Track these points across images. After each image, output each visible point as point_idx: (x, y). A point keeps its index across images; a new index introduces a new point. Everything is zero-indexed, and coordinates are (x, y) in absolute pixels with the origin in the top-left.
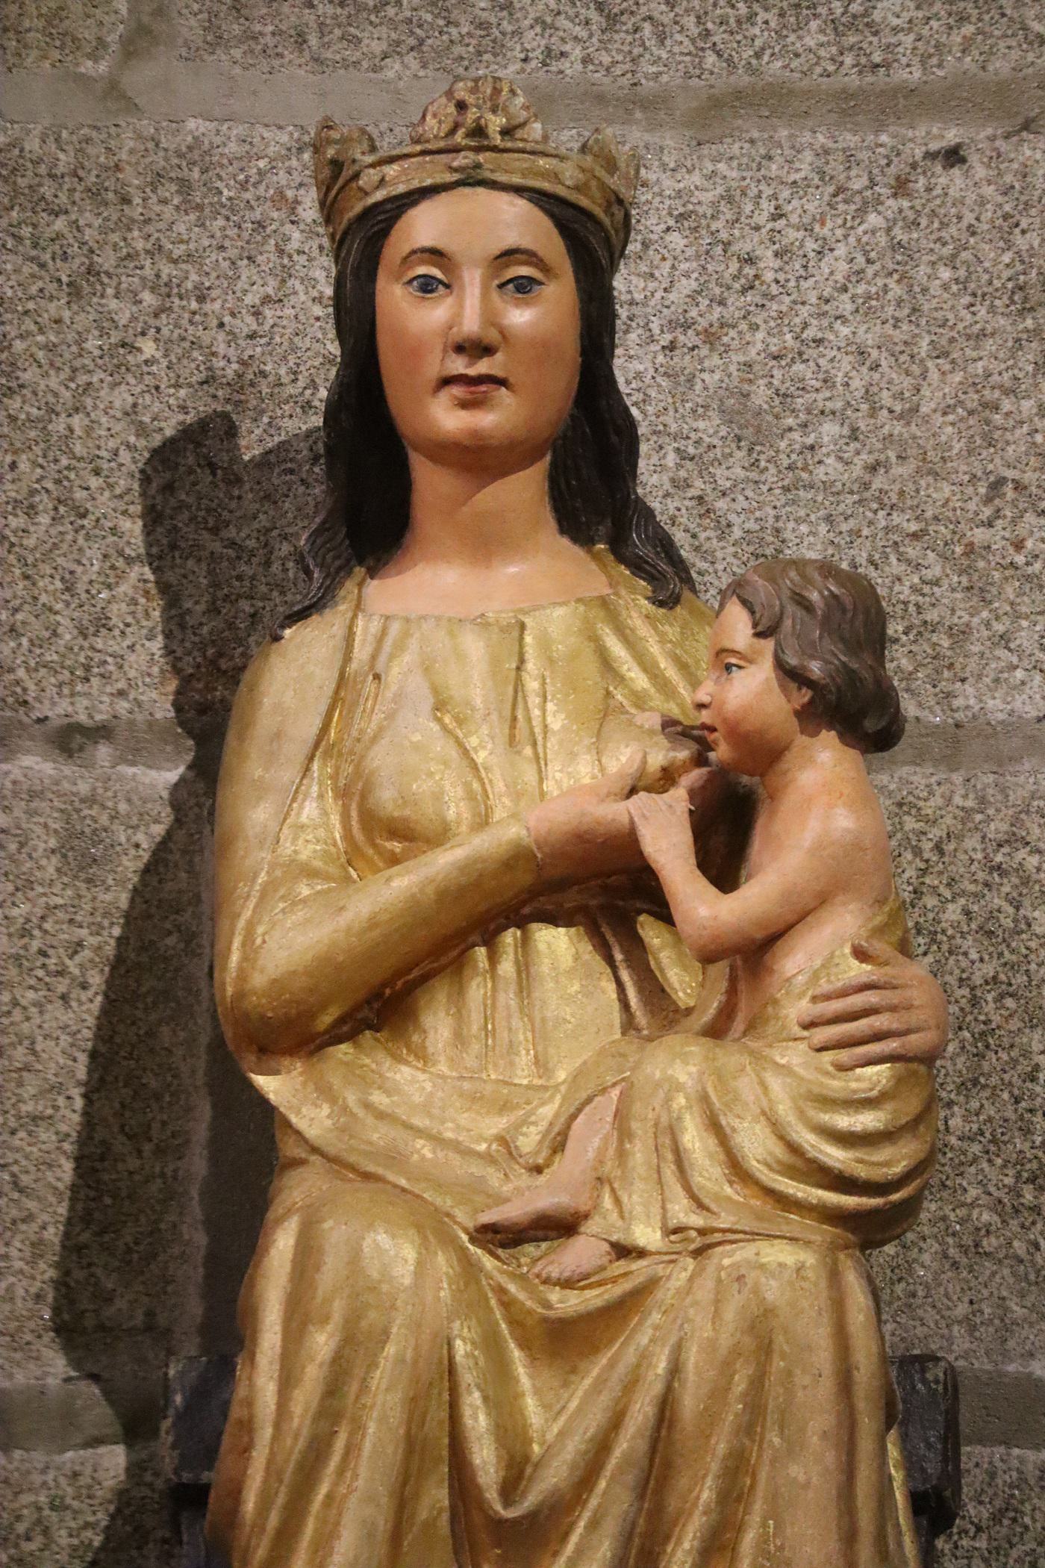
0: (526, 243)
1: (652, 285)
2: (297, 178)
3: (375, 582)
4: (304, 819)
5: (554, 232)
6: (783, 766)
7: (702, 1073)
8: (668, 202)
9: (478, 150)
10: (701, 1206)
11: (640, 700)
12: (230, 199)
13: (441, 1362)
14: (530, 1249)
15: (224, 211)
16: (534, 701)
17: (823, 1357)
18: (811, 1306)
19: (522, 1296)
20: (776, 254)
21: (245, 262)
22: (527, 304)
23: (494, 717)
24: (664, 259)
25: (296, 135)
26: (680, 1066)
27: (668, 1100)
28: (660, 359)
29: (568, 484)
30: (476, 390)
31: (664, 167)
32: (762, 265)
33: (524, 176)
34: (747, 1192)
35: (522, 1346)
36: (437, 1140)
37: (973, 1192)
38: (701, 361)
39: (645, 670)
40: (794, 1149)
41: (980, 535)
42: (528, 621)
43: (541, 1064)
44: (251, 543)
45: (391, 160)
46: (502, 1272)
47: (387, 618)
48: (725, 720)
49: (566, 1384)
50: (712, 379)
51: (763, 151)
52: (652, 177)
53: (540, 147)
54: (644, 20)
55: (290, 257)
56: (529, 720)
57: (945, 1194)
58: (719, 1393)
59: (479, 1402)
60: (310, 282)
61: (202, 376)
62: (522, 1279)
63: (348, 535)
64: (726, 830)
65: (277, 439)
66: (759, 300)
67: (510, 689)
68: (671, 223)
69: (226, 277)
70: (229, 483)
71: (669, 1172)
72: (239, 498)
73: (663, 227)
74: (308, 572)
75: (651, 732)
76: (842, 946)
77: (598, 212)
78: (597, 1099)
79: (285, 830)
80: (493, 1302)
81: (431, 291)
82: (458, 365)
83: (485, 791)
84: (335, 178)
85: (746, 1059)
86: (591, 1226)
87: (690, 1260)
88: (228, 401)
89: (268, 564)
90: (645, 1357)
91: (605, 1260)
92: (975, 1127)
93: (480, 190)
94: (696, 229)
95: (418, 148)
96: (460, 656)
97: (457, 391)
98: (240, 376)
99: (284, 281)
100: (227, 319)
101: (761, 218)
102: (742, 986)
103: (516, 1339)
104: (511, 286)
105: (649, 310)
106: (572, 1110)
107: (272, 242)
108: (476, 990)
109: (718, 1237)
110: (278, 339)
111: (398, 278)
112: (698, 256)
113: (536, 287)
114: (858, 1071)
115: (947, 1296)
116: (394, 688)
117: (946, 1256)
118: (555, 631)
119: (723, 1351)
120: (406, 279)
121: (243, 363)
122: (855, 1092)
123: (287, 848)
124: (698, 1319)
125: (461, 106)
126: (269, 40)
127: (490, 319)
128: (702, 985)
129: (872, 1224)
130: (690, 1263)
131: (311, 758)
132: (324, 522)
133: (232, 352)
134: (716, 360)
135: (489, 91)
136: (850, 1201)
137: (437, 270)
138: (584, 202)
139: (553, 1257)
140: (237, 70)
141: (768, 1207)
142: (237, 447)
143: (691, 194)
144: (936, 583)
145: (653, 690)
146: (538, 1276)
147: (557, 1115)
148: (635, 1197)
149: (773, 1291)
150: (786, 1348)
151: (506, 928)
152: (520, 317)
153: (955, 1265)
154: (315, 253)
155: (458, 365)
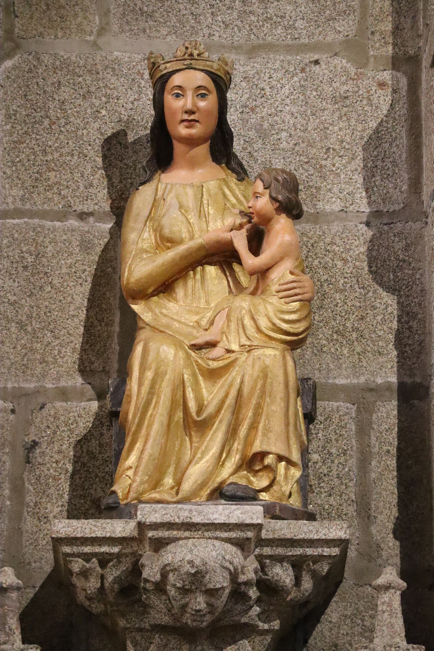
0: (203, 84)
1: (237, 96)
4: (144, 237)
5: (211, 82)
9: (191, 60)
11: (233, 206)
14: (204, 350)
16: (206, 206)
17: (281, 379)
19: (202, 363)
22: (204, 100)
23: (195, 210)
26: (244, 303)
27: (241, 312)
28: (239, 115)
30: (191, 123)
36: (180, 322)
37: (321, 336)
38: (250, 116)
39: (235, 198)
40: (274, 324)
41: (323, 163)
42: (204, 185)
43: (207, 302)
44: (131, 164)
49: (213, 386)
52: (237, 67)
56: (204, 211)
57: (313, 336)
58: (253, 388)
64: (255, 246)
68: (242, 79)
71: (241, 331)
74: (146, 172)
75: (236, 214)
77: (223, 76)
79: (140, 240)
80: (194, 364)
82: (186, 117)
84: (153, 67)
85: (261, 301)
86: (220, 345)
89: (135, 170)
90: (234, 379)
91: (224, 354)
93: (192, 70)
95: (175, 59)
96: (186, 194)
97: (185, 123)
99: (140, 95)
100: (125, 105)
101: (266, 78)
102: (260, 281)
103: (200, 374)
108: (190, 283)
109: (254, 347)
112: (249, 88)
119: (255, 377)
121: (129, 116)
123: (140, 245)
125: (187, 48)
127: (194, 104)
128: (250, 281)
130: (246, 354)
131: (146, 221)
133: (126, 114)
136: (289, 338)
138: (219, 74)
140: (128, 39)
141: (267, 340)
142: (127, 139)
144: (312, 175)
147: (211, 315)
149: (268, 362)
152: (202, 104)
153: (316, 355)
154: (148, 87)
155: (186, 117)
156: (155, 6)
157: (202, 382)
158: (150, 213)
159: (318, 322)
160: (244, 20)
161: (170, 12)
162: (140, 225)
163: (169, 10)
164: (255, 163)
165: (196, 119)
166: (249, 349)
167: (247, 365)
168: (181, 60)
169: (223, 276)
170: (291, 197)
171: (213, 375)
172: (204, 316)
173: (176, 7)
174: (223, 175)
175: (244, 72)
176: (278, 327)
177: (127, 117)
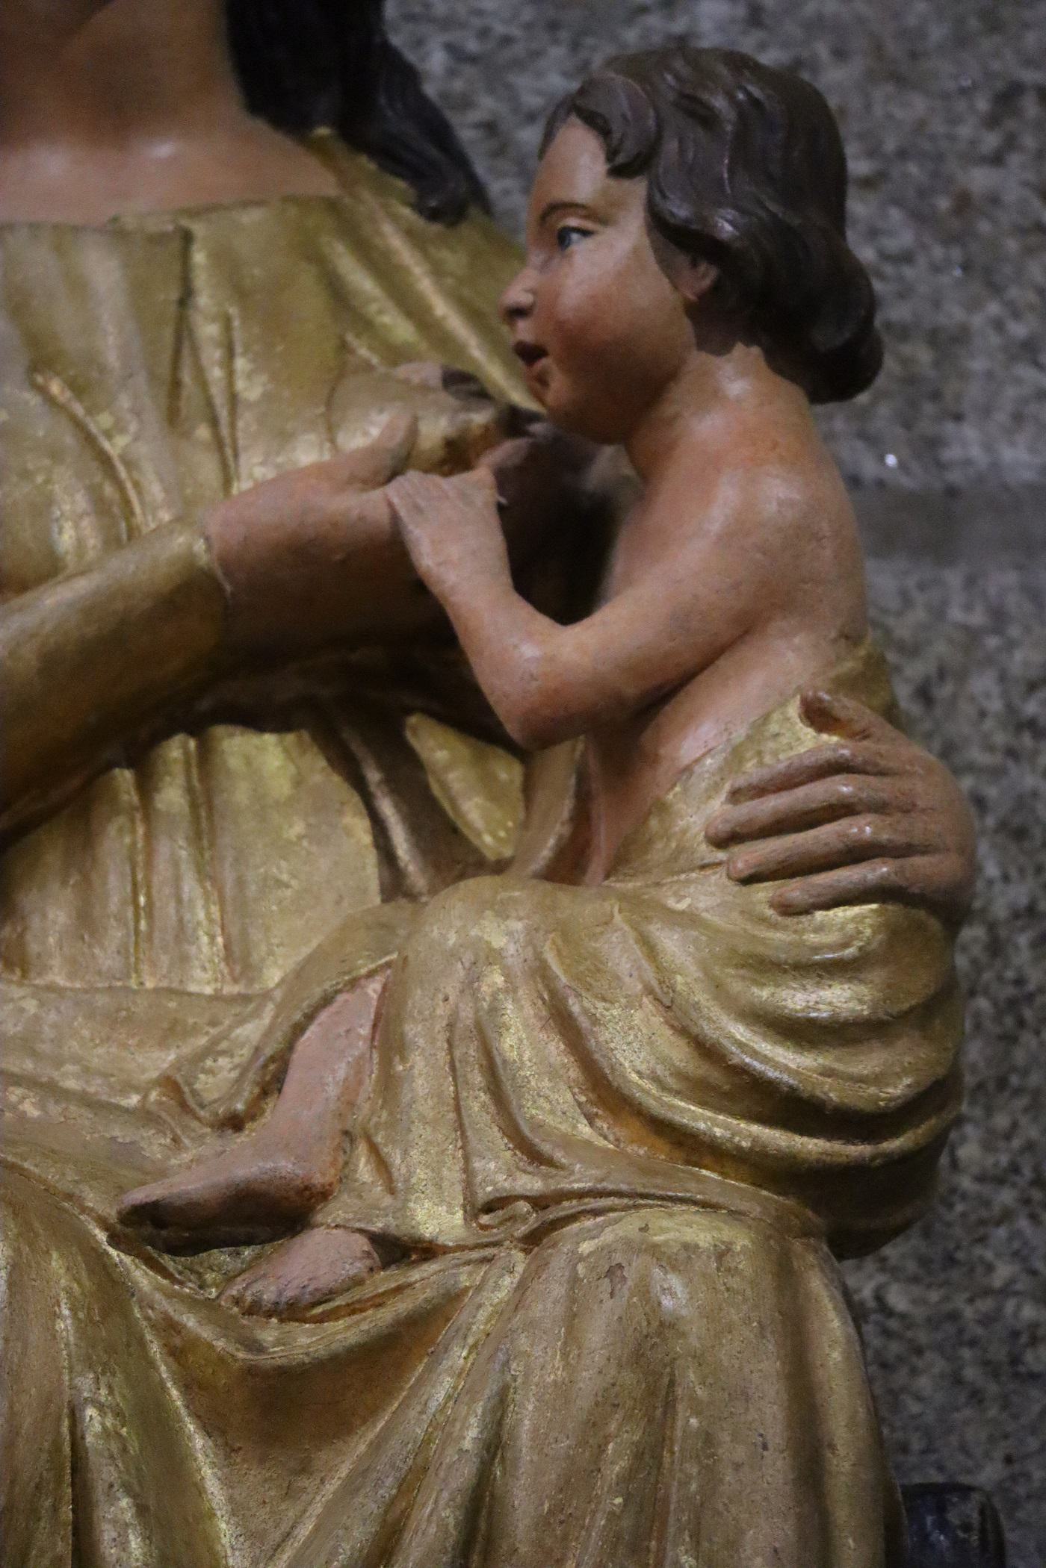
6: (668, 410)
7: (532, 931)
10: (535, 1157)
13: (57, 1447)
14: (221, 1257)
16: (211, 356)
17: (769, 1412)
18: (747, 1321)
19: (206, 1333)
23: (141, 379)
26: (484, 933)
27: (471, 985)
34: (621, 1132)
35: (208, 1429)
36: (50, 1090)
37: (1003, 1271)
40: (707, 1050)
41: (979, 179)
42: (198, 229)
43: (239, 959)
46: (170, 1296)
49: (290, 1493)
56: (203, 383)
57: (955, 1274)
58: (577, 1479)
59: (129, 1516)
62: (209, 1308)
64: (562, 553)
67: (168, 334)
71: (478, 1104)
75: (424, 388)
76: (783, 704)
78: (341, 998)
80: (155, 1349)
83: (126, 502)
85: (613, 906)
86: (335, 1212)
87: (518, 1256)
90: (443, 1427)
91: (359, 1267)
92: (1004, 1159)
96: (79, 287)
102: (600, 807)
103: (197, 1416)
106: (298, 1016)
108: (116, 840)
109: (569, 1207)
114: (819, 915)
115: (964, 1448)
117: (957, 1380)
119: (583, 1403)
122: (816, 949)
124: (538, 1352)
128: (525, 825)
129: (853, 1193)
130: (520, 1260)
136: (811, 1146)
139: (264, 1268)
141: (663, 1154)
144: (906, 258)
146: (237, 1301)
147: (268, 1033)
148: (414, 1153)
149: (675, 1295)
150: (700, 1392)
151: (167, 734)
153: (976, 1396)
157: (207, 1472)
159: (981, 1179)
166: (534, 1221)
167: (531, 1325)
169: (336, 784)
170: (796, 222)
171: (287, 1412)
172: (215, 1042)
176: (742, 1070)
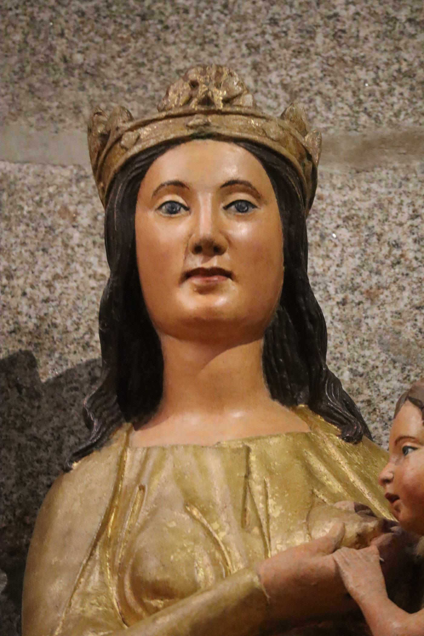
0: (242, 177)
1: (328, 263)
2: (76, 198)
3: (139, 432)
4: (89, 589)
5: (264, 172)
8: (337, 209)
9: (208, 113)
11: (335, 498)
12: (29, 212)
15: (25, 220)
16: (259, 499)
20: (415, 241)
21: (41, 252)
22: (246, 219)
23: (230, 508)
24: (336, 246)
25: (75, 171)
28: (336, 310)
29: (277, 361)
30: (209, 279)
31: (334, 187)
32: (405, 248)
33: (240, 131)
38: (365, 311)
39: (339, 480)
42: (252, 446)
44: (48, 437)
45: (145, 124)
47: (148, 449)
48: (405, 487)
50: (373, 323)
51: (402, 175)
52: (325, 193)
53: (250, 111)
54: (316, 94)
55: (73, 249)
56: (256, 510)
60: (86, 264)
61: (12, 327)
63: (118, 401)
65: (65, 368)
66: (404, 271)
67: (241, 491)
68: (340, 222)
69: (27, 263)
70: (31, 397)
72: (39, 407)
73: (334, 225)
74: (89, 425)
75: (347, 512)
77: (295, 160)
79: (75, 597)
81: (175, 213)
82: (197, 262)
83: (225, 560)
84: (103, 144)
88: (30, 344)
89: (60, 451)
93: (210, 142)
94: (357, 226)
95: (164, 114)
96: (204, 471)
97: (196, 281)
98: (37, 327)
99: (68, 264)
100: (28, 290)
101: (403, 218)
104: (233, 207)
105: (327, 279)
107: (60, 239)
110: (64, 302)
111: (150, 207)
112: (359, 244)
113: (251, 209)
116: (155, 494)
118: (271, 453)
120: (157, 206)
121: (41, 319)
123: (77, 608)
125: (194, 85)
126: (55, 112)
127: (218, 228)
131: (94, 546)
132: (101, 389)
133: (32, 312)
134: (375, 310)
135: (214, 73)
137: (179, 199)
138: (284, 151)
140: (33, 131)
142: (37, 374)
143: (353, 203)
145: (346, 494)
152: (241, 230)
154: (90, 246)
155: (197, 262)
156: (104, 52)
158: (105, 524)
160: (339, 79)
161: (143, 65)
162: (77, 557)
163: (140, 60)
164: (384, 428)
165: (226, 267)
168: (179, 116)
173: (159, 52)
174: (304, 427)
175: (345, 203)
177: (34, 321)
